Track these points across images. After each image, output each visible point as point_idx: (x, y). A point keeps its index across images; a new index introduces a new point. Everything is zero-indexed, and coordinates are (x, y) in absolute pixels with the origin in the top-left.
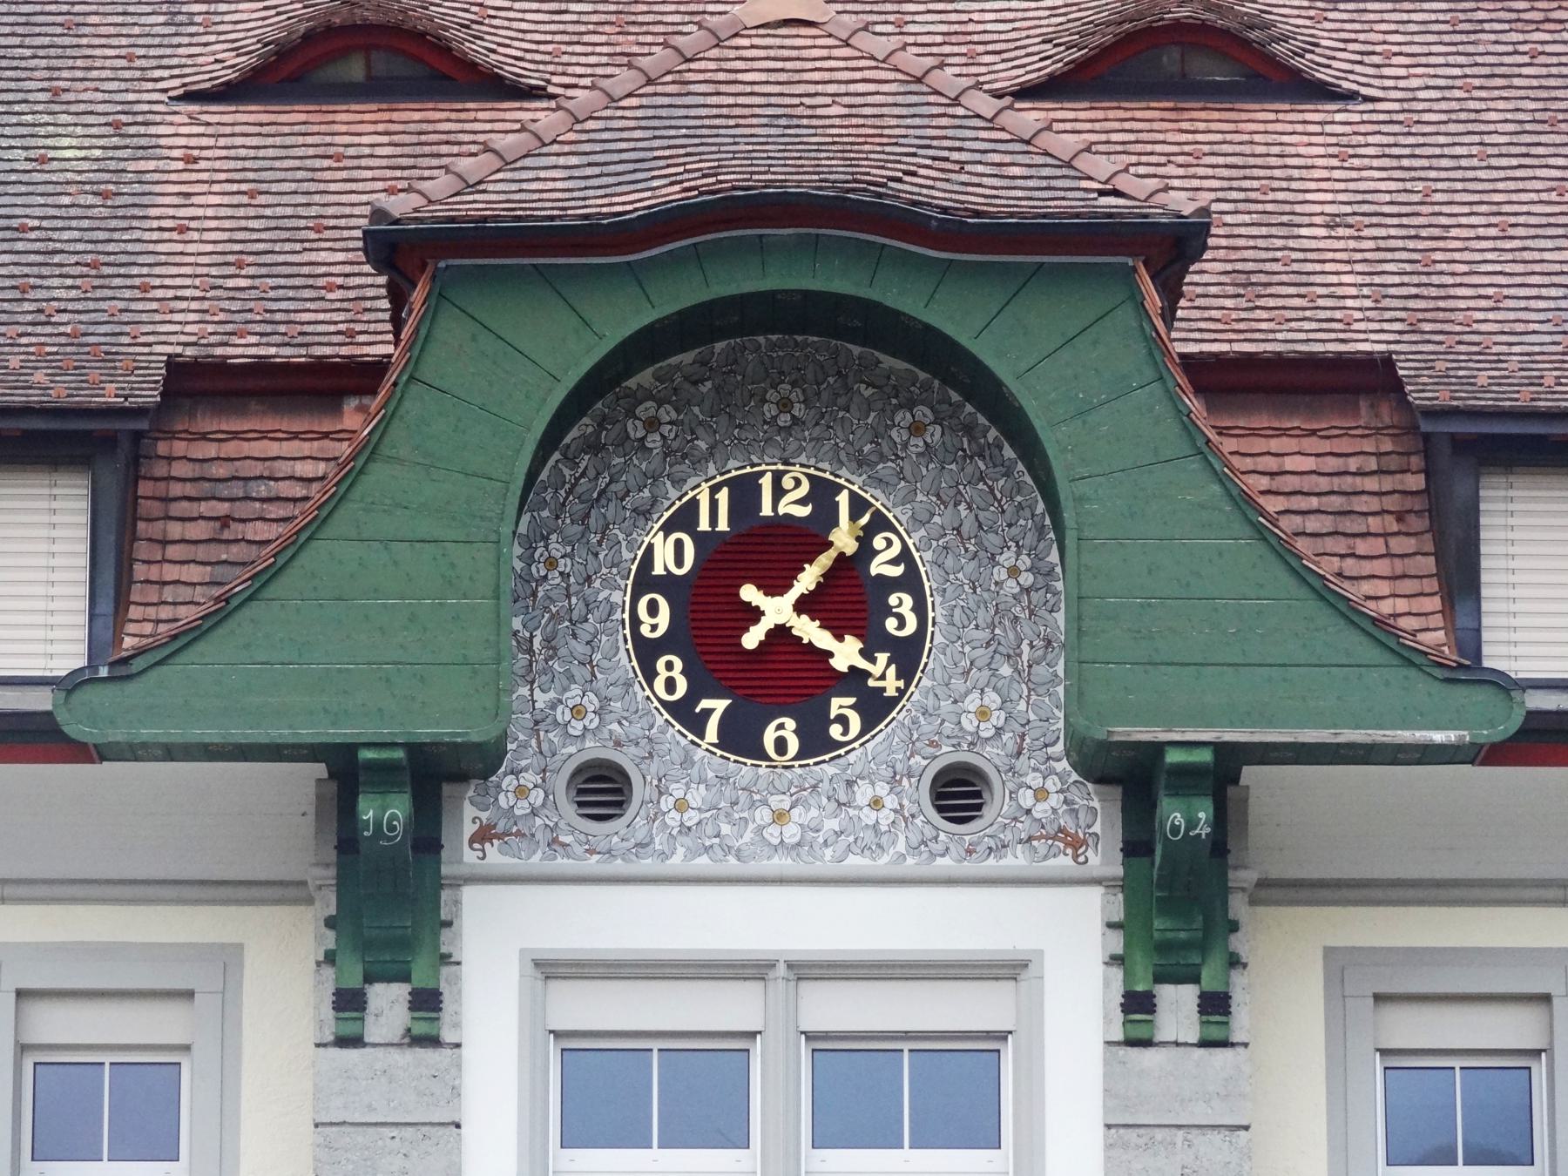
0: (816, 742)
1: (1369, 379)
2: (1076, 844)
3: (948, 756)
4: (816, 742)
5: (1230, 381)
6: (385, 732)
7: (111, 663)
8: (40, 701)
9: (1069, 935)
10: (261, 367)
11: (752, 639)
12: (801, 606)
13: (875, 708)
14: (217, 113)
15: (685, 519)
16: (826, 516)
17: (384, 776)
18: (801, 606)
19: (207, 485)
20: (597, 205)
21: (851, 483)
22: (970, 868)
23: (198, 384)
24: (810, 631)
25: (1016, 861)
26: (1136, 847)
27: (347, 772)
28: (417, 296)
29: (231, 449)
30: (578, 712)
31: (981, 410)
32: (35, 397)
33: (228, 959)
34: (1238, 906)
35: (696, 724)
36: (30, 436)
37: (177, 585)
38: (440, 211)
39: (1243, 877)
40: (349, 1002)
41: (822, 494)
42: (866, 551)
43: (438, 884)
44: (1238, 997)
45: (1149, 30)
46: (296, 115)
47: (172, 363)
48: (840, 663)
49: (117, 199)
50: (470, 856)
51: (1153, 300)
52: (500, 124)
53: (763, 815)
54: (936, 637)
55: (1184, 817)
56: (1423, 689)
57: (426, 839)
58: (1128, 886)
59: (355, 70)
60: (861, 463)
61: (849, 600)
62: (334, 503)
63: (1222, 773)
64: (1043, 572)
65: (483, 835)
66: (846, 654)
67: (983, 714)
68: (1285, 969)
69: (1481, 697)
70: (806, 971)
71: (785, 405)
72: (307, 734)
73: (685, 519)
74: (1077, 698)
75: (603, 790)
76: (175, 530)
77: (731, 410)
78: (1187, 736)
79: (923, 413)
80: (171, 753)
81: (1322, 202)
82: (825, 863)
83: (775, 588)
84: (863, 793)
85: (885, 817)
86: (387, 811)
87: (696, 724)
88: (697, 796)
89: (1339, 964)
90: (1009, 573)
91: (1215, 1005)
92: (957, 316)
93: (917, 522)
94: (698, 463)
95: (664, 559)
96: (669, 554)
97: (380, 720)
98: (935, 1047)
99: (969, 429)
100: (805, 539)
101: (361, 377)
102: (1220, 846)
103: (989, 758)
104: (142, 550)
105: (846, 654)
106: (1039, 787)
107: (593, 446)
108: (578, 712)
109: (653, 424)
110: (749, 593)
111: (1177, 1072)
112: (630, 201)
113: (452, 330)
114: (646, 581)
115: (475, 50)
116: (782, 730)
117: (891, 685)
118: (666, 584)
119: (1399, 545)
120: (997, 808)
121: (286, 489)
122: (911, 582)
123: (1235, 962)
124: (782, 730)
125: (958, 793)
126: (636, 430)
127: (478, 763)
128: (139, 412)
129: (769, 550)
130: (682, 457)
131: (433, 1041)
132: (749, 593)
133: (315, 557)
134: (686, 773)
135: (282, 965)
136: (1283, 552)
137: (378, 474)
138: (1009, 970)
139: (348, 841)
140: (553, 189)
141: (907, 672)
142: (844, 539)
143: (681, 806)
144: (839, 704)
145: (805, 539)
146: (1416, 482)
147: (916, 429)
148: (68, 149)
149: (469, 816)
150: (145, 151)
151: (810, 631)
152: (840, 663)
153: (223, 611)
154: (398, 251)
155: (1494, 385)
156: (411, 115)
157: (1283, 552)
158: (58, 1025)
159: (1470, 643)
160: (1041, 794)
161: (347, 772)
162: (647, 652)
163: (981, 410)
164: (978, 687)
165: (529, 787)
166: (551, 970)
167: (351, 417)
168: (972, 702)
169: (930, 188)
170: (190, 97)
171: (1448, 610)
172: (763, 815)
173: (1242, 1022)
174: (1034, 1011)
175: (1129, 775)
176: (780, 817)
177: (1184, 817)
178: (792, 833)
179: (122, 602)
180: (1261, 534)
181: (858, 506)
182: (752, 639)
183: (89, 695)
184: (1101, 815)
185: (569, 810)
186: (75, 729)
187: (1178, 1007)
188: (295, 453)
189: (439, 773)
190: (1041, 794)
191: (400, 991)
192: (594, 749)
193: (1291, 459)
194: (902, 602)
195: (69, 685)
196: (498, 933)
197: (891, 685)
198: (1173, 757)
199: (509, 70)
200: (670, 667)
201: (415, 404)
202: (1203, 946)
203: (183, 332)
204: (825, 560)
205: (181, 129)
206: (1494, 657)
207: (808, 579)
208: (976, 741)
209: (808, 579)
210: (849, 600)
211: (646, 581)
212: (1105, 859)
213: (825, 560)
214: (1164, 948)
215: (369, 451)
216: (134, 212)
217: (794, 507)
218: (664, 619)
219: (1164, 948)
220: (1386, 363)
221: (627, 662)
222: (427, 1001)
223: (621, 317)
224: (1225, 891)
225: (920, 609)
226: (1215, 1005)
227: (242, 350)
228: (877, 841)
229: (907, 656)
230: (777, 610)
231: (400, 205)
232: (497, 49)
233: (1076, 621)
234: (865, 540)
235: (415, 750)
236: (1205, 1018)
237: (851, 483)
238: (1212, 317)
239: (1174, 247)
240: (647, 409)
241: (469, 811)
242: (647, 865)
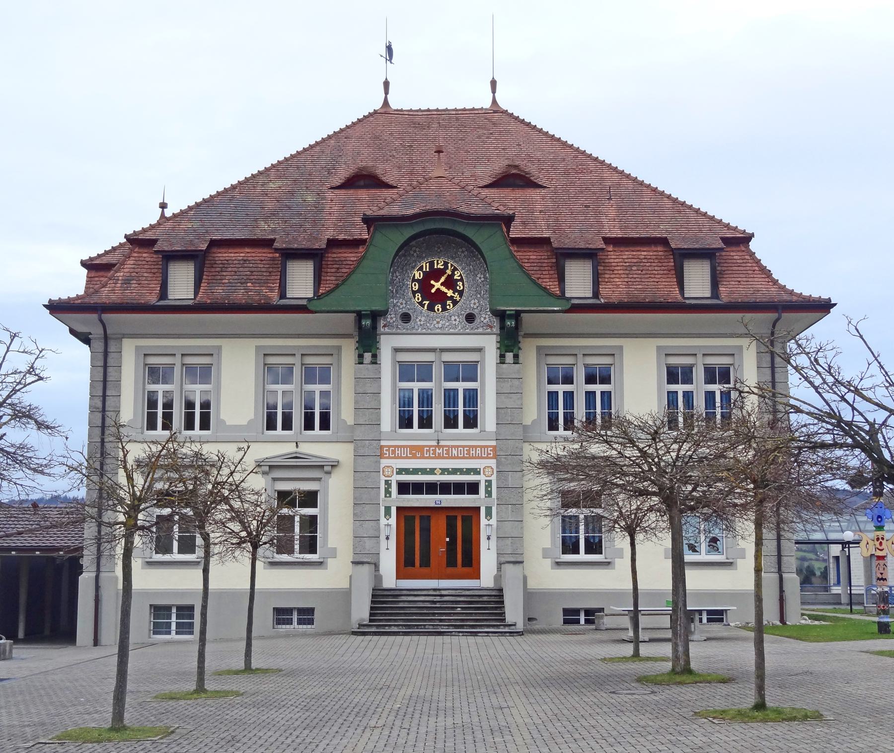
0: (444, 309)
1: (546, 241)
2: (491, 327)
3: (468, 311)
4: (444, 309)
5: (519, 242)
6: (366, 308)
7: (317, 296)
8: (304, 302)
9: (490, 344)
10: (345, 240)
11: (433, 291)
12: (442, 284)
13: (455, 303)
14: (337, 191)
15: (421, 269)
16: (446, 267)
17: (366, 316)
18: (442, 284)
19: (335, 262)
20: (404, 213)
21: (450, 262)
22: (472, 331)
23: (333, 243)
24: (444, 289)
25: (480, 330)
26: (502, 327)
27: (360, 315)
28: (372, 229)
29: (339, 255)
30: (402, 304)
31: (473, 249)
32: (303, 247)
33: (339, 348)
34: (520, 339)
35: (423, 306)
36: (305, 254)
37: (330, 280)
38: (375, 214)
39: (522, 333)
40: (361, 356)
41: (446, 264)
42: (453, 274)
43: (376, 335)
44: (520, 355)
45: (507, 176)
46: (351, 191)
47: (328, 239)
48: (449, 295)
49: (318, 208)
50: (382, 330)
51: (505, 229)
52: (386, 193)
53: (435, 322)
54: (466, 290)
55: (510, 323)
56: (552, 299)
57: (374, 327)
58: (500, 335)
59: (362, 183)
60: (453, 258)
61: (450, 283)
62: (356, 268)
63: (517, 315)
64: (485, 278)
65: (385, 326)
66: (450, 293)
67: (475, 304)
68: (529, 350)
69: (564, 302)
70: (443, 350)
71: (439, 248)
72: (352, 309)
73: (421, 269)
74: (490, 303)
75: (406, 318)
76: (329, 270)
77: (430, 250)
78: (511, 309)
79: (464, 249)
80: (328, 312)
81: (539, 207)
82: (446, 331)
83: (437, 281)
84: (453, 318)
85: (457, 323)
86: (367, 323)
87: (423, 306)
88: (423, 319)
89: (539, 349)
90: (480, 278)
91: (516, 357)
92: (469, 233)
93: (463, 269)
94: (423, 259)
95: (417, 277)
96: (418, 275)
97: (365, 307)
98: (191, 625)
99: (472, 252)
100: (441, 272)
101: (362, 242)
102: (517, 327)
103: (476, 312)
104: (323, 274)
105: (450, 293)
106: (485, 317)
107: (404, 255)
108: (402, 304)
109: (415, 251)
110: (432, 282)
111: (509, 368)
112: (410, 212)
113: (378, 236)
114: (414, 280)
115: (384, 179)
116: (438, 307)
117: (458, 299)
118: (418, 281)
119: (552, 272)
120: (477, 321)
121: (349, 263)
122: (462, 280)
123: (520, 349)
124: (438, 307)
125: (470, 318)
126: (412, 252)
127: (384, 313)
128: (322, 249)
129: (435, 274)
130: (421, 258)
131: (376, 363)
132: (432, 282)
133: (353, 277)
134: (421, 315)
135: (349, 349)
136: (529, 276)
137: (365, 263)
138: (480, 350)
139: (360, 327)
140: (395, 210)
141: (461, 297)
142: (449, 272)
143: (420, 321)
144: (448, 302)
145: (441, 272)
146: (554, 261)
147: (463, 252)
148: (309, 199)
149: (382, 322)
150: (323, 199)
151: (444, 289)
152: (449, 295)
153: (337, 286)
154: (368, 221)
155: (568, 243)
156: (373, 191)
157: (529, 276)
158: (309, 360)
159: (563, 291)
160: (485, 318)
161: (360, 315)
162: (414, 293)
163: (473, 249)
164: (473, 297)
165: (392, 318)
166: (397, 350)
167: (361, 249)
168: (473, 302)
169: (464, 209)
170: (332, 188)
171: (559, 284)
172: (435, 322)
173: (521, 359)
174: (483, 359)
175: (501, 316)
176: (438, 323)
177: (510, 323)
178: (440, 325)
179: (319, 284)
180: (524, 272)
181: (452, 265)
182: (433, 291)
183: (314, 302)
184: (496, 322)
185: (400, 322)
186: (311, 308)
187: (509, 356)
188: (351, 256)
189: (375, 316)
190: (485, 318)
191: (370, 354)
192: (404, 310)
193: (532, 256)
194: (460, 283)
195: (309, 300)
196: (387, 344)
197: (458, 299)
198: (508, 312)
199: (390, 183)
200: (418, 296)
201: (371, 249)
202: (514, 346)
203: (330, 234)
204: (446, 276)
205: (330, 195)
206: (567, 295)
207: (443, 279)
208: (474, 309)
209: (443, 279)
210: (450, 283)
211: (414, 280)
212: (496, 330)
213: (446, 276)
214: (507, 346)
215: (363, 257)
216: (321, 210)
217: (440, 266)
218: (417, 287)
219: (507, 346)
220: (549, 239)
221: (410, 294)
222: (375, 356)
223: (408, 233)
224: (518, 336)
225: (463, 285)
226: (516, 357)
227: (341, 237)
228: (456, 327)
229: (461, 293)
230: (437, 285)
231: (369, 213)
232: (388, 179)
233: (491, 288)
234: (453, 271)
235: (372, 311)
236: (47, 632)
237: (450, 262)
238: (516, 232)
239: (508, 220)
240: (414, 248)
241: (382, 322)
242: (414, 331)
